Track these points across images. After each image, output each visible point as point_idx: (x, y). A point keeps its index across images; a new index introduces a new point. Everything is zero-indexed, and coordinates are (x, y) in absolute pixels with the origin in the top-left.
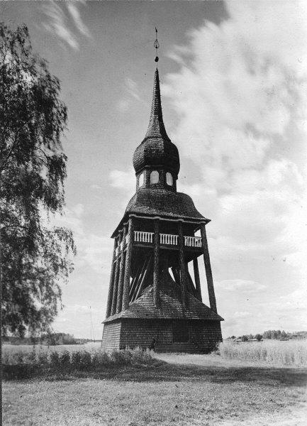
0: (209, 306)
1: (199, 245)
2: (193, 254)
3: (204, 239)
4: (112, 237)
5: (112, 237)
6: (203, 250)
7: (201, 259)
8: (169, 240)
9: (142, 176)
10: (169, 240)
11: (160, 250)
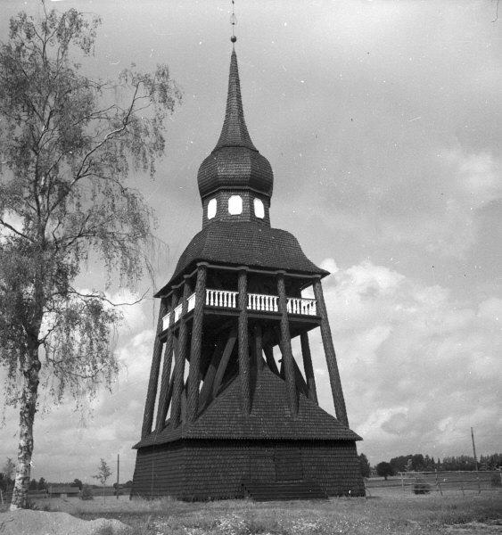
0: (335, 416)
1: (313, 312)
2: (301, 326)
3: (320, 302)
4: (157, 296)
5: (157, 296)
6: (319, 320)
7: (314, 335)
8: (263, 303)
10: (263, 303)
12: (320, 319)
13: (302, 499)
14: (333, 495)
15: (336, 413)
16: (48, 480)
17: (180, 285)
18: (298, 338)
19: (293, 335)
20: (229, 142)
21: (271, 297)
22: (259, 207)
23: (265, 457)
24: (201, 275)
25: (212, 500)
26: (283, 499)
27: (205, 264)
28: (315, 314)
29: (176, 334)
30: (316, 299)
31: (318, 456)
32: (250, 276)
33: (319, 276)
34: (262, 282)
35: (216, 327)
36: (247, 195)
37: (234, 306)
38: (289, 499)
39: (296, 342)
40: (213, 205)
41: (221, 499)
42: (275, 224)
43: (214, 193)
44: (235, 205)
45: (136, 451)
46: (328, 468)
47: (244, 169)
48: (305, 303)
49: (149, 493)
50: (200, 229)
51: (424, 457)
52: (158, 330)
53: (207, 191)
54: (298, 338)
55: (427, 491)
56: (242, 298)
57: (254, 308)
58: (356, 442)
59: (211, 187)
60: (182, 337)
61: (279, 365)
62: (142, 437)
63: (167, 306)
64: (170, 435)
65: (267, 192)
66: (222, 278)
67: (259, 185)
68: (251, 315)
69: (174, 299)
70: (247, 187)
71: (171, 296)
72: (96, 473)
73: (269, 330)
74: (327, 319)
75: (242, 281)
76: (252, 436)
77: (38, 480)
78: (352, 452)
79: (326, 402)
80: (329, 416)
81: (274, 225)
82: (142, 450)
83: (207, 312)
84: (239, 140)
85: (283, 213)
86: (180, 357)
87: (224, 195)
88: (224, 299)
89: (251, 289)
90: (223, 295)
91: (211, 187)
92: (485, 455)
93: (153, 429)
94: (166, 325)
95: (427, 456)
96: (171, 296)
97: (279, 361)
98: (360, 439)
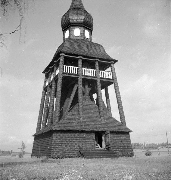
0: (120, 122)
2: (105, 84)
3: (113, 74)
4: (43, 72)
5: (43, 72)
7: (111, 88)
8: (89, 72)
9: (67, 32)
10: (89, 72)
11: (83, 79)
12: (114, 80)
13: (106, 157)
14: (120, 156)
15: (121, 120)
16: (13, 151)
17: (53, 66)
18: (104, 89)
19: (102, 89)
20: (74, 7)
21: (93, 70)
22: (87, 33)
23: (89, 139)
24: (62, 59)
25: (66, 158)
26: (98, 158)
27: (63, 54)
28: (111, 78)
29: (51, 87)
30: (112, 71)
31: (110, 140)
32: (83, 61)
33: (113, 62)
34: (89, 63)
35: (69, 83)
36: (82, 28)
37: (76, 73)
38: (101, 158)
39: (103, 91)
40: (67, 33)
41: (70, 157)
42: (94, 40)
43: (69, 27)
44: (77, 32)
45: (34, 137)
46: (118, 144)
47: (80, 18)
48: (107, 74)
49: (38, 155)
50: (62, 42)
51: (140, 144)
52: (44, 86)
53: (66, 27)
54: (104, 89)
55: (150, 154)
56: (80, 71)
57: (85, 74)
58: (130, 133)
59: (67, 25)
60: (53, 87)
61: (95, 101)
62: (37, 131)
63: (47, 77)
64: (47, 129)
65: (91, 28)
66: (71, 61)
67: (88, 25)
68: (84, 77)
69: (50, 73)
70: (82, 25)
71: (49, 72)
72: (20, 147)
73: (91, 84)
74: (116, 80)
75: (80, 62)
76: (83, 129)
77: (10, 151)
78: (128, 137)
79: (115, 115)
80: (118, 121)
81: (93, 41)
82: (37, 137)
83: (64, 75)
84: (79, 6)
85: (97, 36)
86: (52, 97)
87: (72, 28)
88: (72, 70)
89: (84, 66)
90: (70, 68)
91: (67, 25)
92: (160, 143)
93: (41, 128)
94: (47, 84)
95: (141, 143)
96: (49, 72)
97: (95, 100)
98: (131, 132)
